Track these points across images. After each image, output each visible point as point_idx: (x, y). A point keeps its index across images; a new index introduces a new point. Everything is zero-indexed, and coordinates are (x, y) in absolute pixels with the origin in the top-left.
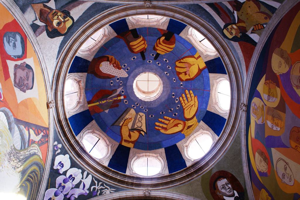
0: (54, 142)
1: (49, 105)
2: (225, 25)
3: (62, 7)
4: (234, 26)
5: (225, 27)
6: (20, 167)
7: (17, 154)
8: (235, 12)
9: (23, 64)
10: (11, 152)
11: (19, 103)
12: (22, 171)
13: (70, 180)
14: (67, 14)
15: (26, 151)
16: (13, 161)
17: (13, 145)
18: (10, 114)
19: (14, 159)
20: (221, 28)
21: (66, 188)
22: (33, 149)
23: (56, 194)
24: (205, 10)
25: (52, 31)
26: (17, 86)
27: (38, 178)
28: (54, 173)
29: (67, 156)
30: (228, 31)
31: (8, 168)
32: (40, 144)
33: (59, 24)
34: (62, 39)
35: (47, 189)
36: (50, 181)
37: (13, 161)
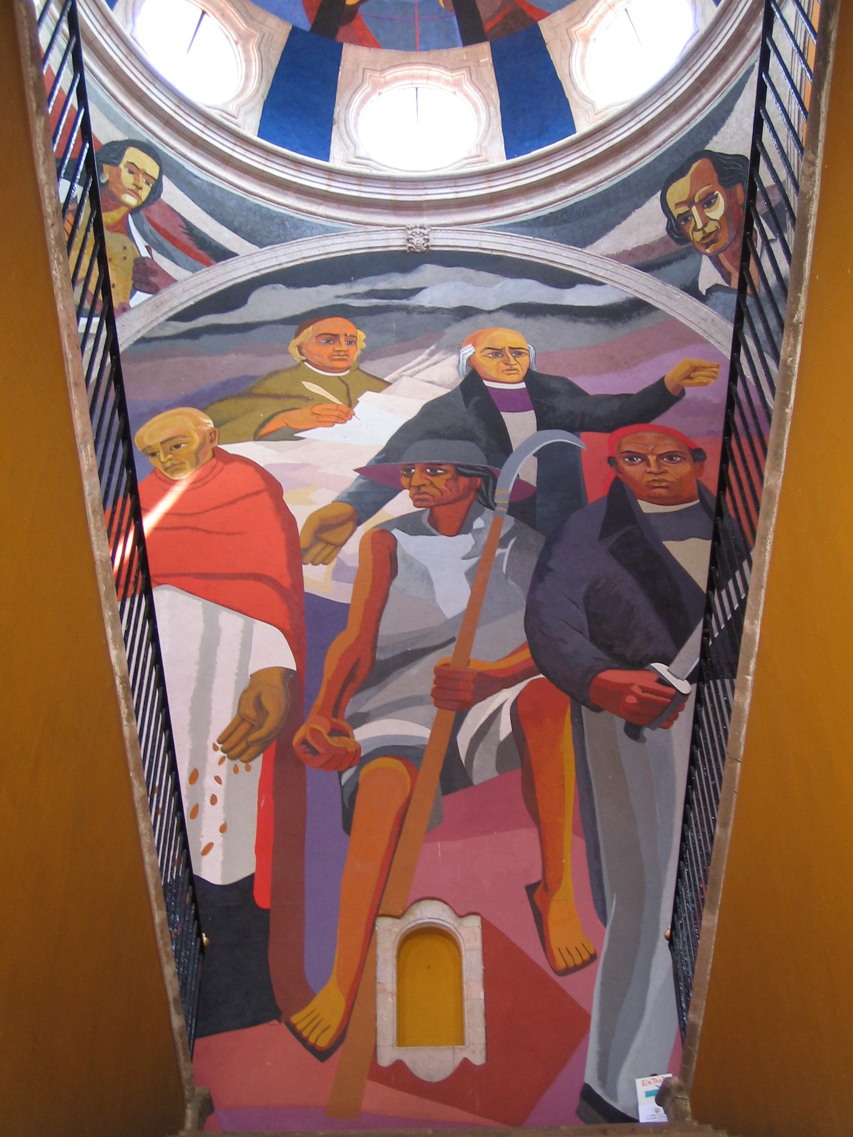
2: (160, 196)
3: (683, 257)
4: (131, 200)
5: (157, 189)
8: (144, 253)
14: (677, 228)
20: (169, 177)
24: (235, 231)
25: (734, 184)
30: (145, 173)
33: (708, 201)
34: (715, 138)
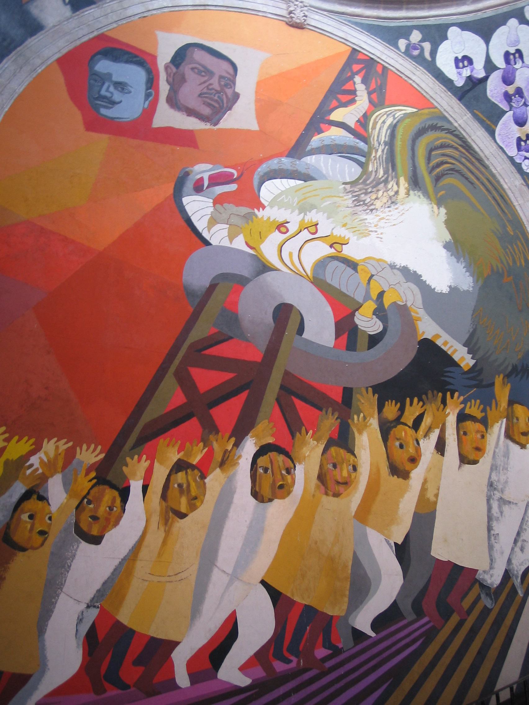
0: (398, 48)
1: (296, 23)
6: (398, 187)
7: (368, 182)
9: (170, 76)
10: (356, 196)
11: (259, 126)
12: (409, 184)
13: (515, 64)
15: (374, 155)
16: (376, 199)
17: (344, 186)
18: (274, 164)
19: (374, 197)
21: (526, 87)
22: (380, 129)
23: (520, 121)
26: (217, 117)
27: (452, 147)
28: (470, 92)
29: (453, 32)
31: (383, 218)
32: (378, 101)
35: (492, 133)
36: (482, 113)
37: (376, 199)
